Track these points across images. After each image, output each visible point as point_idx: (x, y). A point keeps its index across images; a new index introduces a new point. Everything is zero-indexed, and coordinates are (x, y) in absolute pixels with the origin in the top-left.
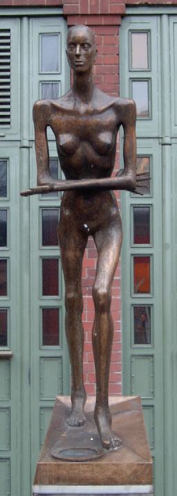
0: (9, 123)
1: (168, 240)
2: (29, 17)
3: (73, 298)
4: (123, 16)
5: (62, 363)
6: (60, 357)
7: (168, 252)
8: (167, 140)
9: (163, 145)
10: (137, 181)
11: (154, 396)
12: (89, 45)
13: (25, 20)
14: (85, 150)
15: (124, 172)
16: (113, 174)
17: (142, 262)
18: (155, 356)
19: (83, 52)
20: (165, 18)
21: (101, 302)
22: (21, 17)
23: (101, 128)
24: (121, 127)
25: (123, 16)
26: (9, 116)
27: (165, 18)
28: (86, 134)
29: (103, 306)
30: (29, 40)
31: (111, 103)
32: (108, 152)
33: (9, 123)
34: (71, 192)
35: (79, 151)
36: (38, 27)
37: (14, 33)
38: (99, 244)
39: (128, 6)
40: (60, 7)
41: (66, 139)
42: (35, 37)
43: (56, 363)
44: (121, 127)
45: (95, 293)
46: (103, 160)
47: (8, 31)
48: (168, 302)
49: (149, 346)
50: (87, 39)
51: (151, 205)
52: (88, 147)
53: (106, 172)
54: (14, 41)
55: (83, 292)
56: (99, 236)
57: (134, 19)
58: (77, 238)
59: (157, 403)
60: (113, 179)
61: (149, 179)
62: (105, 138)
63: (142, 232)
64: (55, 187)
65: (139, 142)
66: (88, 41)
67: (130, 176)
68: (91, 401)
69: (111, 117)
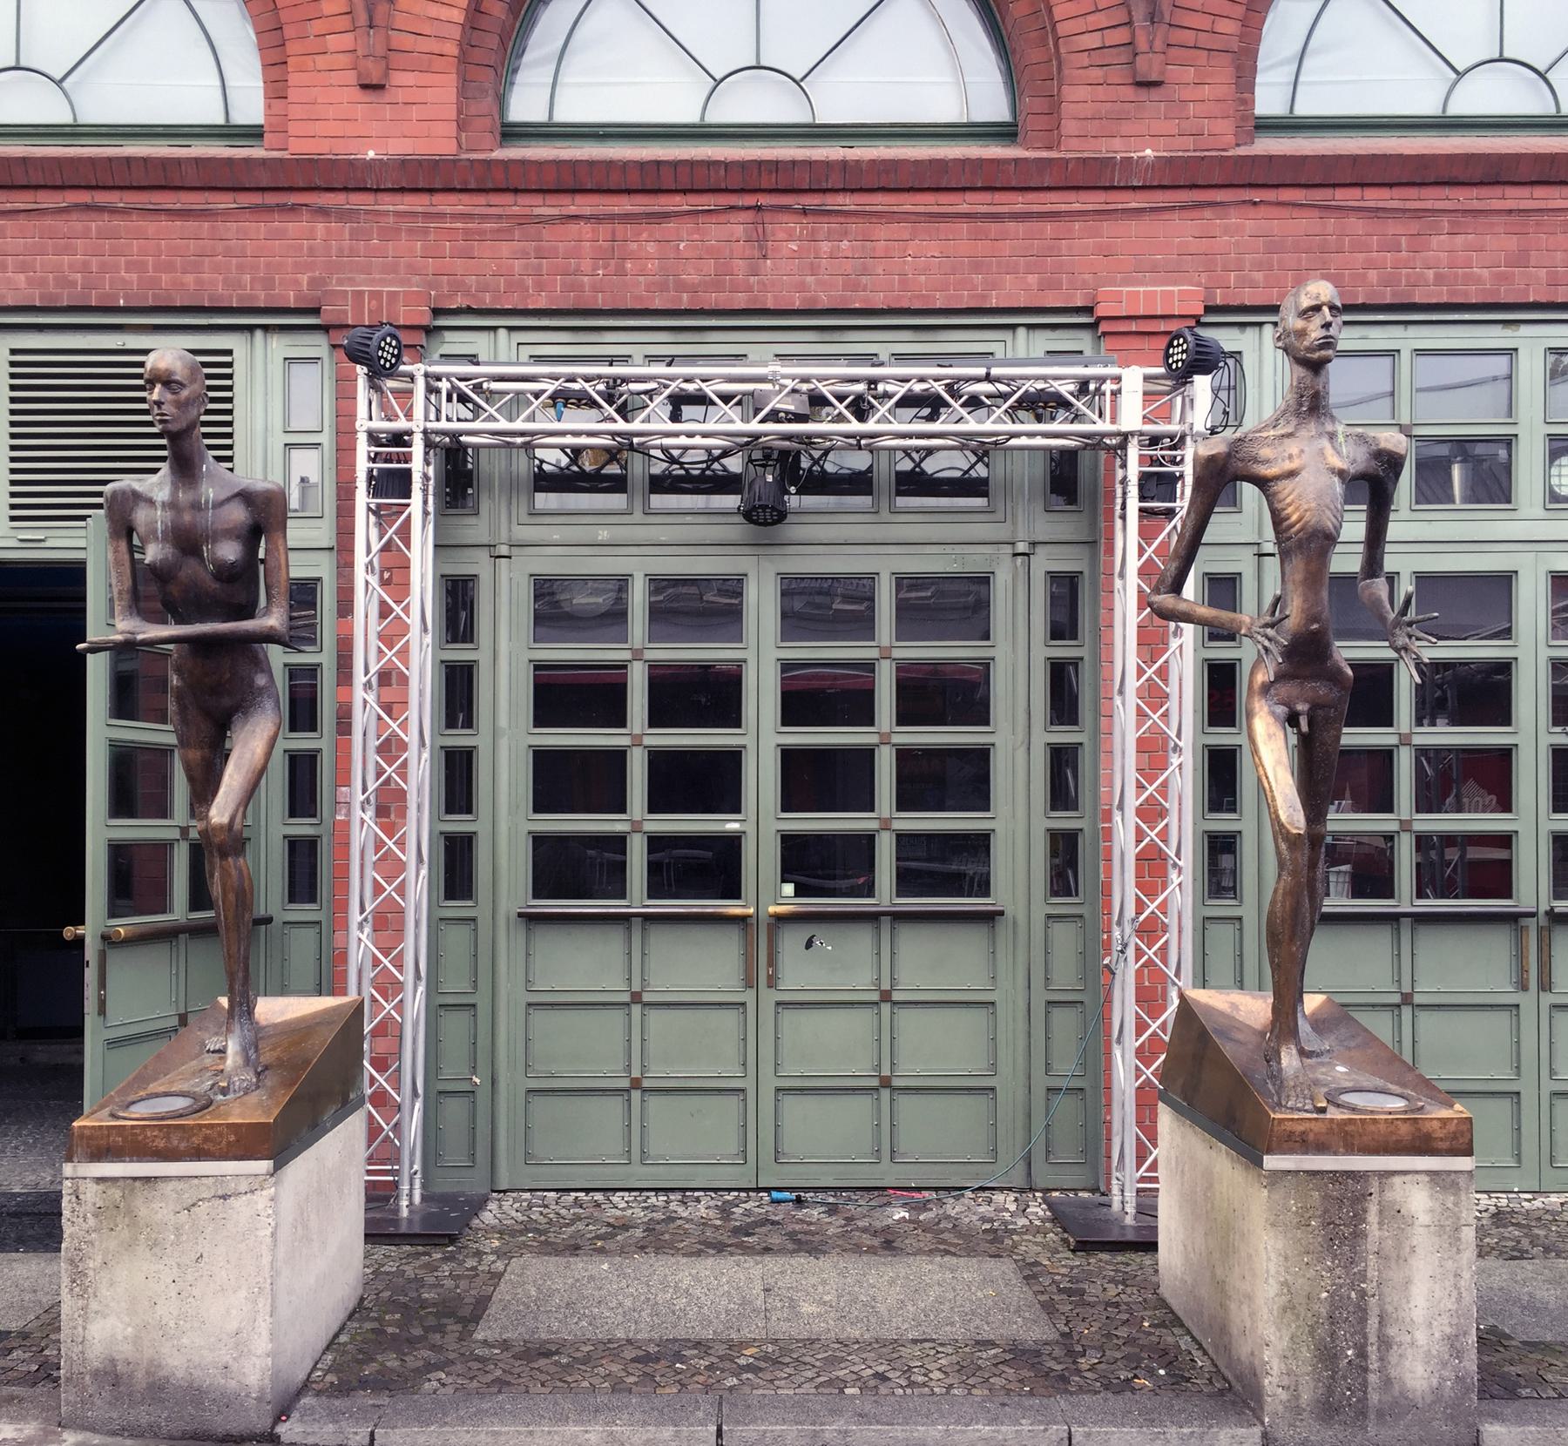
1: (503, 721)
2: (266, 328)
4: (430, 331)
7: (503, 743)
8: (504, 550)
9: (1260, 555)
12: (182, 385)
13: (259, 334)
18: (479, 921)
19: (169, 396)
20: (502, 333)
22: (251, 329)
25: (430, 331)
27: (502, 333)
36: (280, 346)
37: (239, 357)
39: (437, 312)
40: (316, 311)
42: (277, 366)
46: (237, 588)
47: (229, 352)
48: (503, 827)
49: (470, 903)
54: (239, 370)
57: (448, 336)
61: (1555, 612)
63: (303, 713)
65: (1388, 548)
69: (238, 514)
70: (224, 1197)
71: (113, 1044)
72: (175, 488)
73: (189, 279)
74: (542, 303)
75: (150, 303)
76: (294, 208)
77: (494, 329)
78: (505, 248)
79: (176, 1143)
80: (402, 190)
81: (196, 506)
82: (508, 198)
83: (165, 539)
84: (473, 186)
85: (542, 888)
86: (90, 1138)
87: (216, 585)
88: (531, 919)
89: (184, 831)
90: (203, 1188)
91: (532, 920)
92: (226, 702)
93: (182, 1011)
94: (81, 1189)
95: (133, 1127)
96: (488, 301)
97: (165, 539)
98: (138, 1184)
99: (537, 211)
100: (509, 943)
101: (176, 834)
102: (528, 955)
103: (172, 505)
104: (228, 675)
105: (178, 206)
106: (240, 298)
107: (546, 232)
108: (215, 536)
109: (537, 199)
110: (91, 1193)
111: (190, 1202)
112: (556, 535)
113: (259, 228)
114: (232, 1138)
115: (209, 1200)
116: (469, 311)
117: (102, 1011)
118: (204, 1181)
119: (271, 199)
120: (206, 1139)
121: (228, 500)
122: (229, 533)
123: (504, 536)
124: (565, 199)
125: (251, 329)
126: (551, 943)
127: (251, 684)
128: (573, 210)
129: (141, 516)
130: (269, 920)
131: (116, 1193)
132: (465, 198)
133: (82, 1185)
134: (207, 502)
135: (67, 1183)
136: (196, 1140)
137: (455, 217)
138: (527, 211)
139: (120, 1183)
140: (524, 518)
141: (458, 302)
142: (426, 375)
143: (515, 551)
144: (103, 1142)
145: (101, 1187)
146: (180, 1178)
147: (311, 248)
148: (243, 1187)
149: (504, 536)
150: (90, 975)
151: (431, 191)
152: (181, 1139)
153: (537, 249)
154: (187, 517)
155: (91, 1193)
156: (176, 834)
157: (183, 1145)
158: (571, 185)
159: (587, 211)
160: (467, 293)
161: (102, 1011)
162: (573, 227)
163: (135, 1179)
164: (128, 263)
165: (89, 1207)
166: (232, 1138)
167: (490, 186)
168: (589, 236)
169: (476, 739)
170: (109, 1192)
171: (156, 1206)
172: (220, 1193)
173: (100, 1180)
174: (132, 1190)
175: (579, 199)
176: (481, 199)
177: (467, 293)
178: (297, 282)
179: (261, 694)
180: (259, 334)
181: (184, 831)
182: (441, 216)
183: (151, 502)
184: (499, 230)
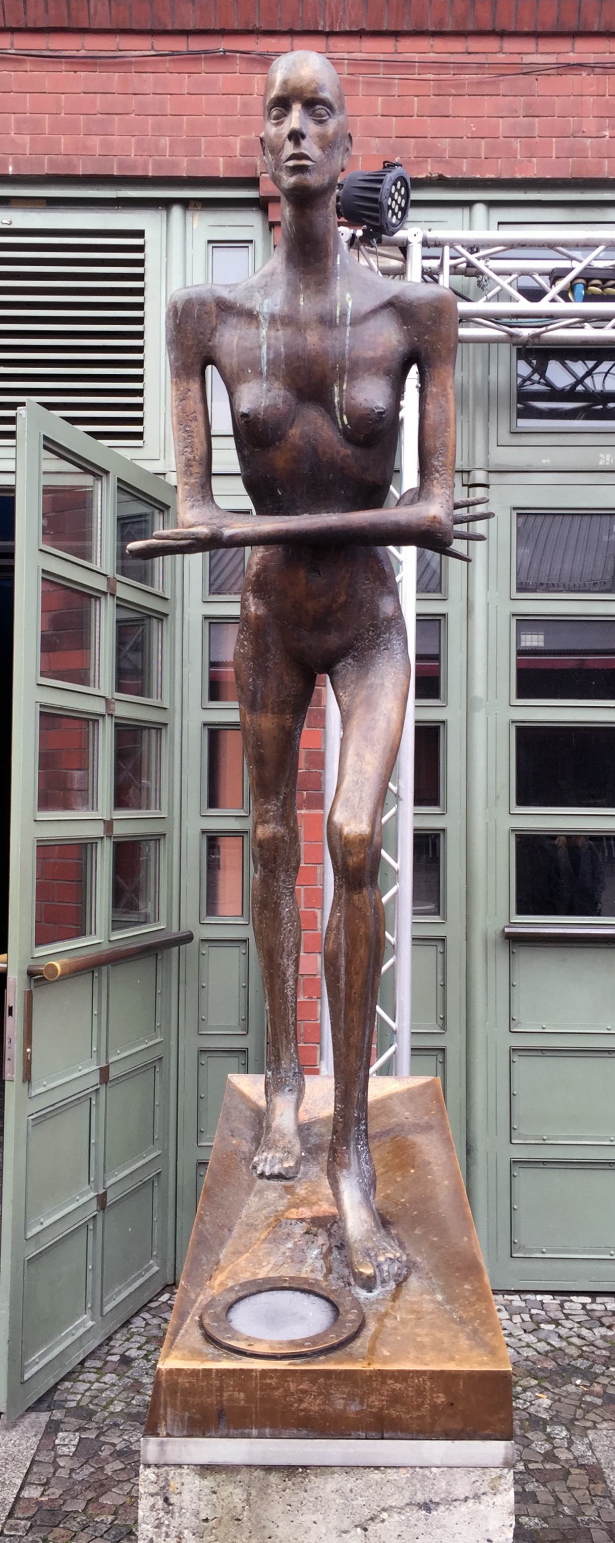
0: (139, 436)
1: (479, 690)
3: (274, 838)
5: (247, 954)
6: (245, 941)
7: (479, 718)
10: (458, 521)
11: (444, 1026)
13: (177, 211)
14: (313, 427)
15: (421, 493)
16: (390, 501)
17: (429, 738)
18: (449, 941)
20: (480, 209)
21: (352, 861)
23: (354, 369)
24: (414, 369)
26: (139, 407)
28: (310, 381)
29: (360, 869)
30: (185, 254)
31: (386, 297)
32: (378, 434)
33: (139, 436)
34: (273, 550)
35: (295, 432)
37: (152, 240)
38: (345, 699)
40: (253, 182)
41: (256, 396)
42: (199, 248)
43: (234, 954)
44: (414, 369)
45: (333, 832)
47: (140, 234)
50: (320, 88)
51: (444, 615)
52: (320, 421)
53: (374, 494)
54: (152, 256)
55: (298, 800)
56: (346, 666)
58: (286, 678)
59: (453, 1042)
60: (391, 514)
62: (371, 394)
64: (227, 532)
66: (326, 95)
67: (434, 509)
68: (320, 1093)
69: (387, 337)
70: (427, 1507)
71: (41, 1119)
72: (293, 291)
73: (96, 142)
74: (534, 171)
75: (46, 170)
76: (225, 56)
77: (469, 204)
78: (487, 105)
79: (339, 1404)
80: (360, 34)
81: (327, 322)
82: (491, 44)
83: (273, 374)
84: (449, 28)
85: (530, 899)
86: (187, 1392)
87: (347, 451)
88: (515, 941)
89: (109, 825)
90: (388, 1489)
91: (516, 941)
92: (333, 640)
93: (104, 1065)
94: (174, 1484)
95: (264, 1373)
96: (465, 170)
97: (273, 374)
98: (274, 1478)
99: (527, 59)
100: (490, 970)
101: (98, 830)
102: (511, 985)
103: (286, 320)
104: (343, 599)
105: (83, 53)
106: (158, 165)
107: (541, 85)
108: (354, 369)
109: (528, 45)
110: (190, 1491)
111: (367, 1513)
112: (545, 458)
113: (183, 81)
114: (441, 1399)
115: (400, 1510)
116: (442, 182)
117: (27, 1077)
118: (392, 1474)
119: (197, 44)
120: (395, 1399)
121: (375, 312)
122: (373, 366)
123: (480, 462)
124: (563, 45)
125: (166, 204)
126: (537, 967)
127: (374, 614)
128: (572, 58)
129: (231, 339)
130: (189, 938)
131: (234, 1494)
132: (439, 44)
133: (175, 1478)
134: (343, 315)
135: (147, 1475)
136: (375, 1401)
137: (425, 65)
138: (516, 59)
139: (243, 1476)
140: (506, 438)
141: (428, 170)
142: (425, 243)
143: (494, 478)
144: (212, 1400)
145: (209, 1482)
146: (348, 1469)
147: (245, 105)
148: (462, 1488)
149: (480, 462)
150: (13, 1026)
151: (396, 34)
152: (351, 1397)
153: (528, 106)
154: (313, 339)
155: (190, 1491)
156: (98, 830)
157: (354, 1408)
158: (573, 26)
159: (592, 59)
160: (439, 159)
161: (27, 1077)
162: (573, 80)
163: (269, 1469)
164: (18, 122)
165: (188, 1520)
166: (441, 1399)
167: (471, 27)
168: (593, 90)
169: (448, 712)
170: (225, 1491)
171: (307, 1519)
172: (420, 1498)
173: (206, 1469)
174: (264, 1489)
175: (582, 45)
176: (457, 45)
177: (439, 159)
178: (228, 146)
179: (388, 629)
180: (177, 211)
181: (109, 825)
182: (408, 65)
183: (250, 316)
184: (480, 83)
